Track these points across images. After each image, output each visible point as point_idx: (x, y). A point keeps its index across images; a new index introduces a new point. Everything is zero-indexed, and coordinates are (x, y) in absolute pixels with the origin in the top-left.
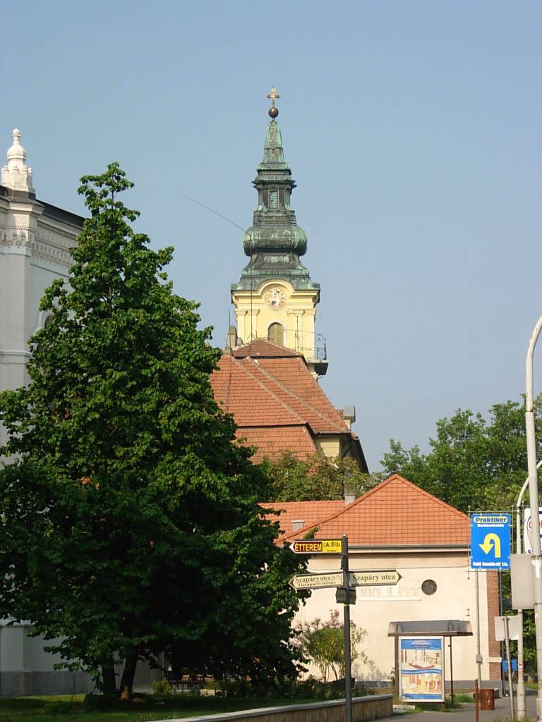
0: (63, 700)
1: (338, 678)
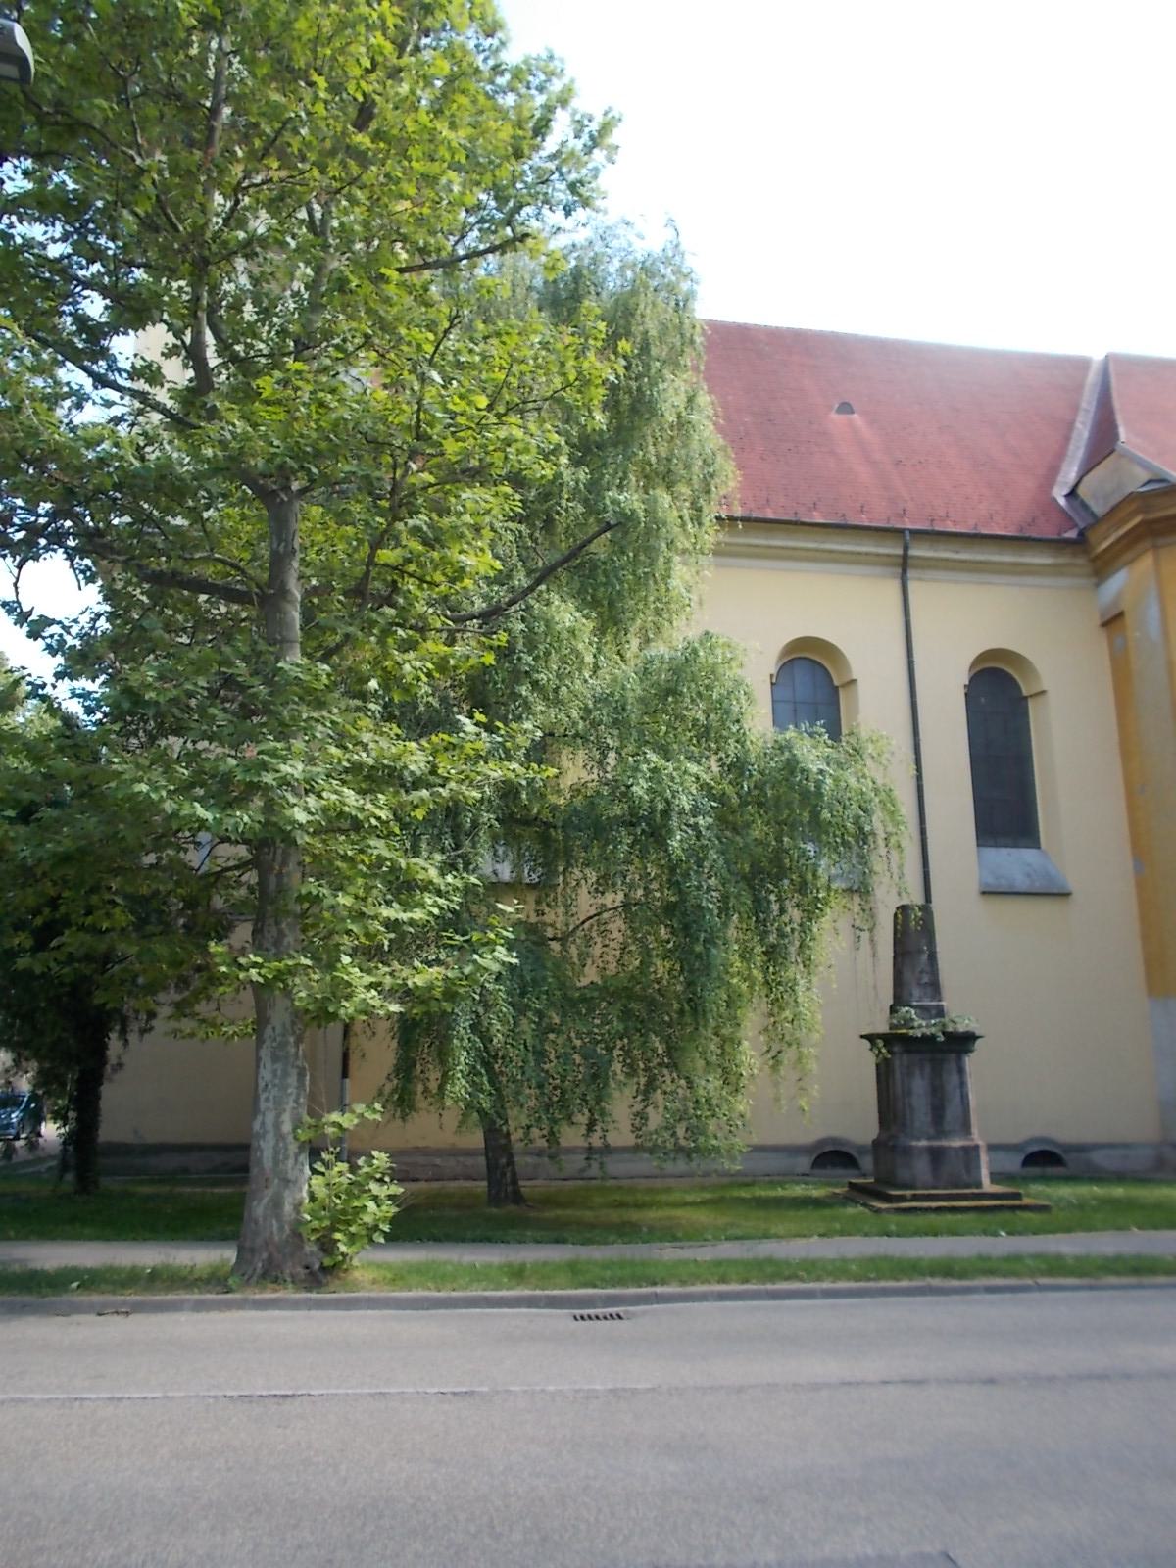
0: (38, 1265)
1: (523, 1189)
